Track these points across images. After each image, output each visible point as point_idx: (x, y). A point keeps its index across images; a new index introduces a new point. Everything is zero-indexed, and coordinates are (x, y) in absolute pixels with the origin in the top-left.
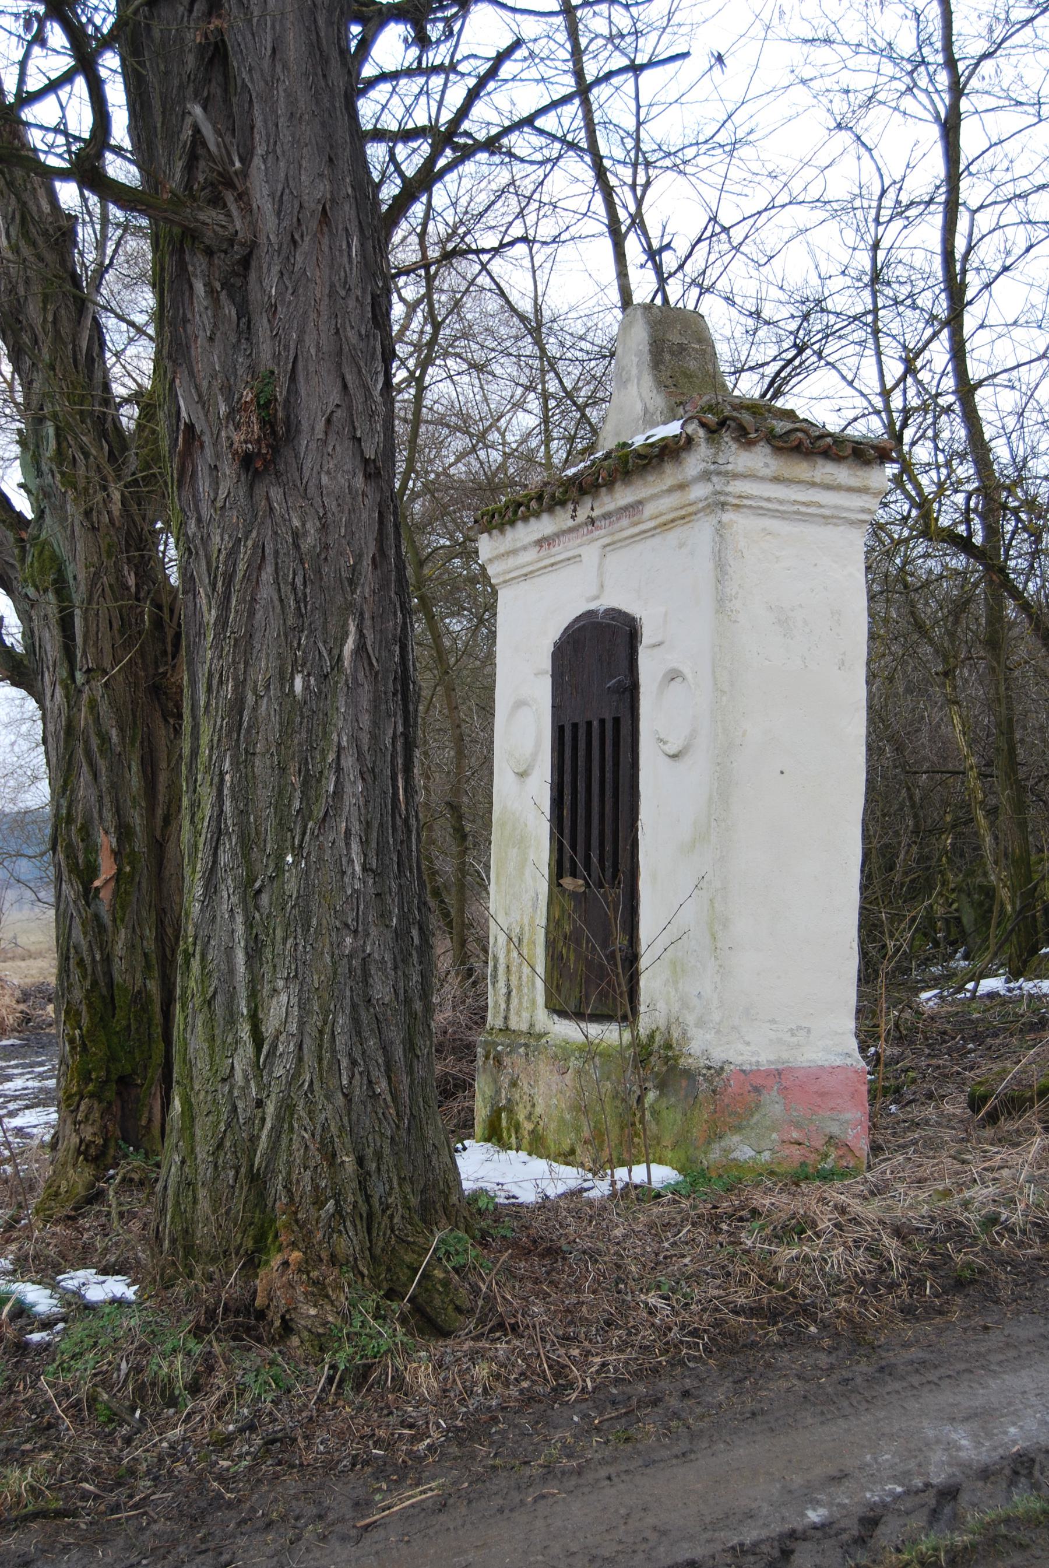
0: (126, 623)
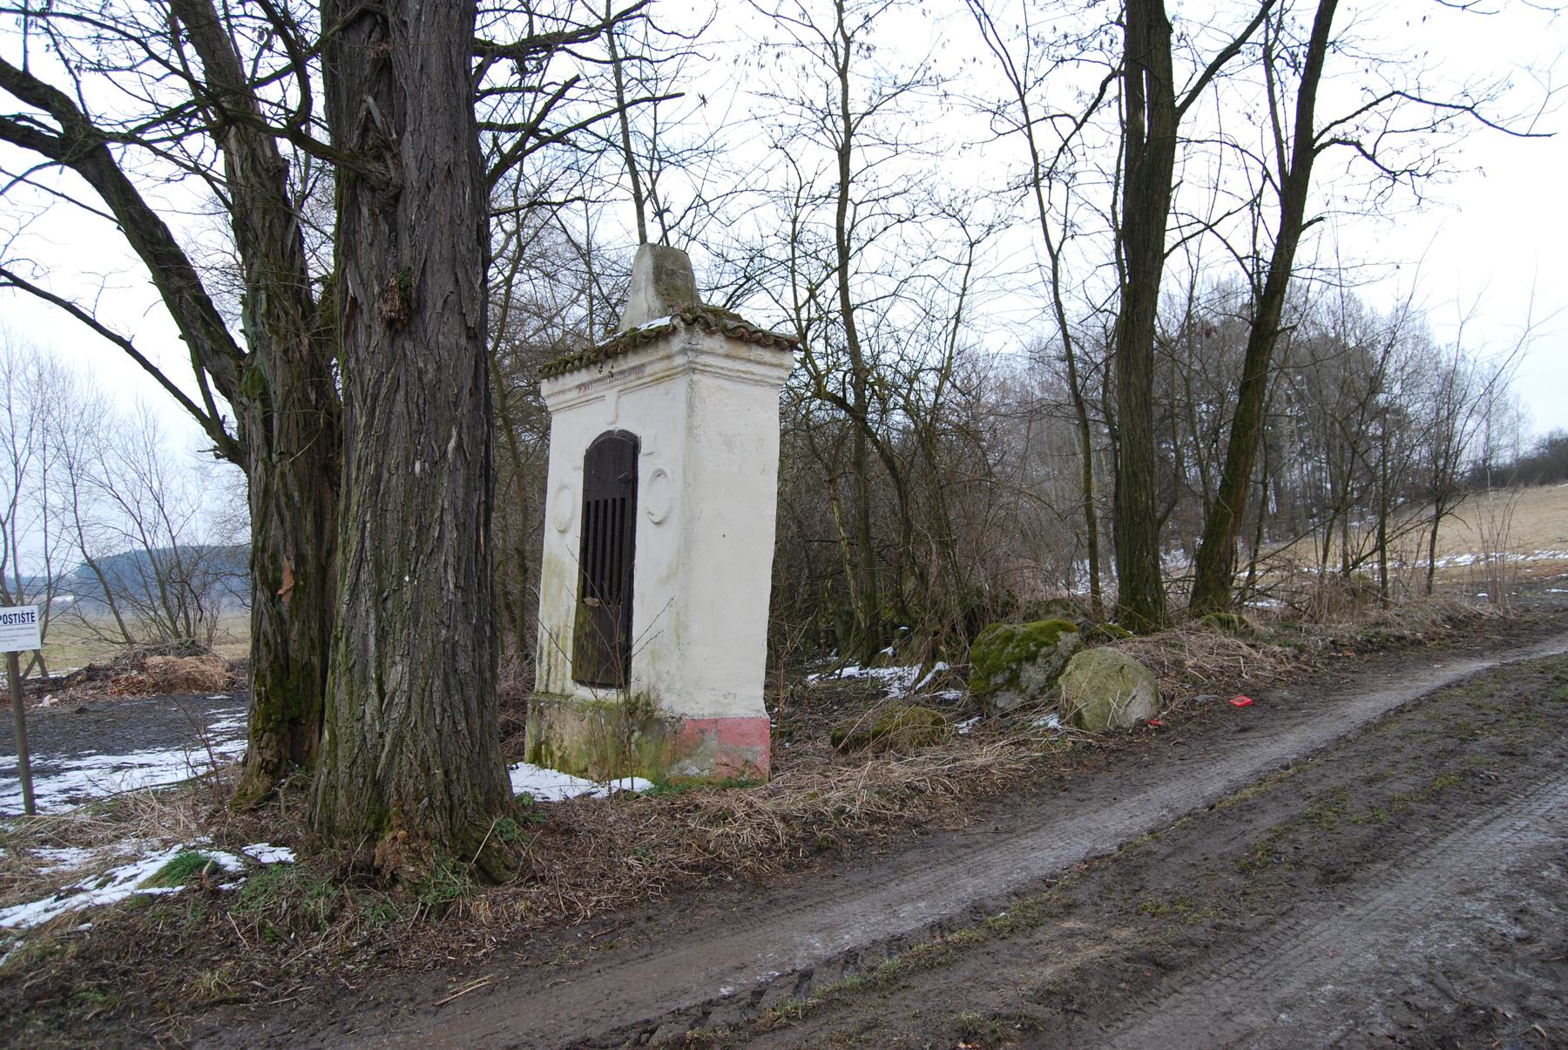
0: (308, 424)
